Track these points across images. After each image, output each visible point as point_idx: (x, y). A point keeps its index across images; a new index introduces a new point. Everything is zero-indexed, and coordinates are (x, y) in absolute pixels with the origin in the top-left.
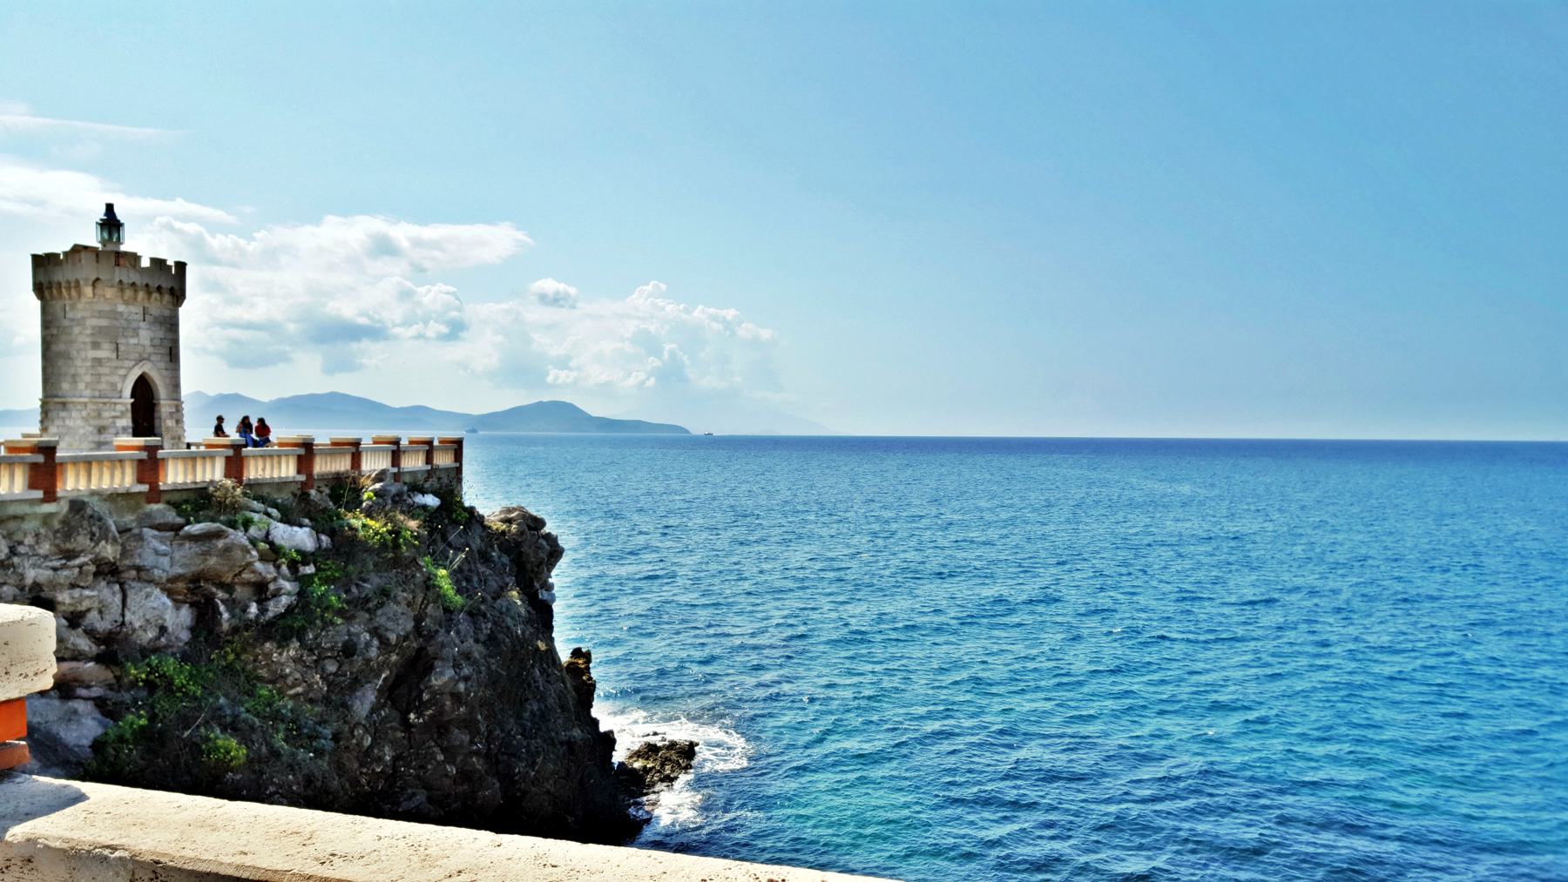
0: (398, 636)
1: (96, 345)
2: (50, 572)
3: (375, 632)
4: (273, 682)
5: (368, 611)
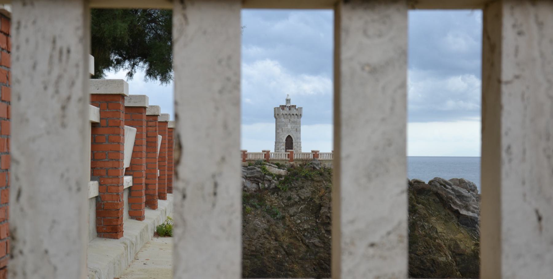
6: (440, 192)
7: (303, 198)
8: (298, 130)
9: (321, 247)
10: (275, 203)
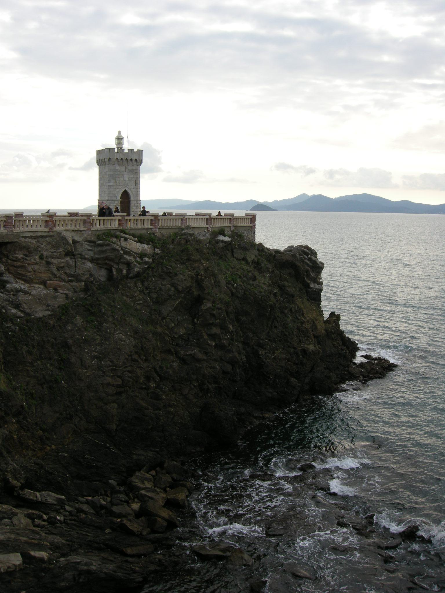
0: (183, 288)
1: (109, 181)
2: (50, 253)
3: (173, 285)
4: (131, 298)
5: (170, 277)
6: (298, 263)
7: (180, 288)
8: (137, 183)
9: (204, 360)
10: (139, 300)
